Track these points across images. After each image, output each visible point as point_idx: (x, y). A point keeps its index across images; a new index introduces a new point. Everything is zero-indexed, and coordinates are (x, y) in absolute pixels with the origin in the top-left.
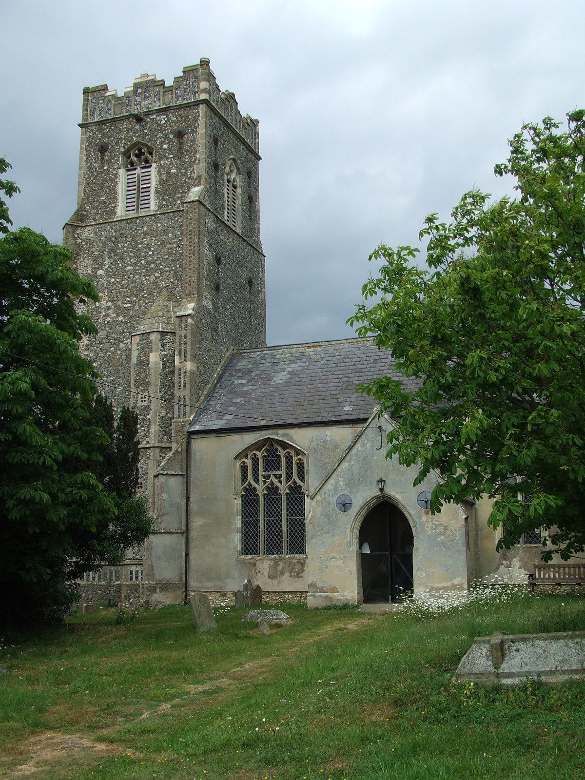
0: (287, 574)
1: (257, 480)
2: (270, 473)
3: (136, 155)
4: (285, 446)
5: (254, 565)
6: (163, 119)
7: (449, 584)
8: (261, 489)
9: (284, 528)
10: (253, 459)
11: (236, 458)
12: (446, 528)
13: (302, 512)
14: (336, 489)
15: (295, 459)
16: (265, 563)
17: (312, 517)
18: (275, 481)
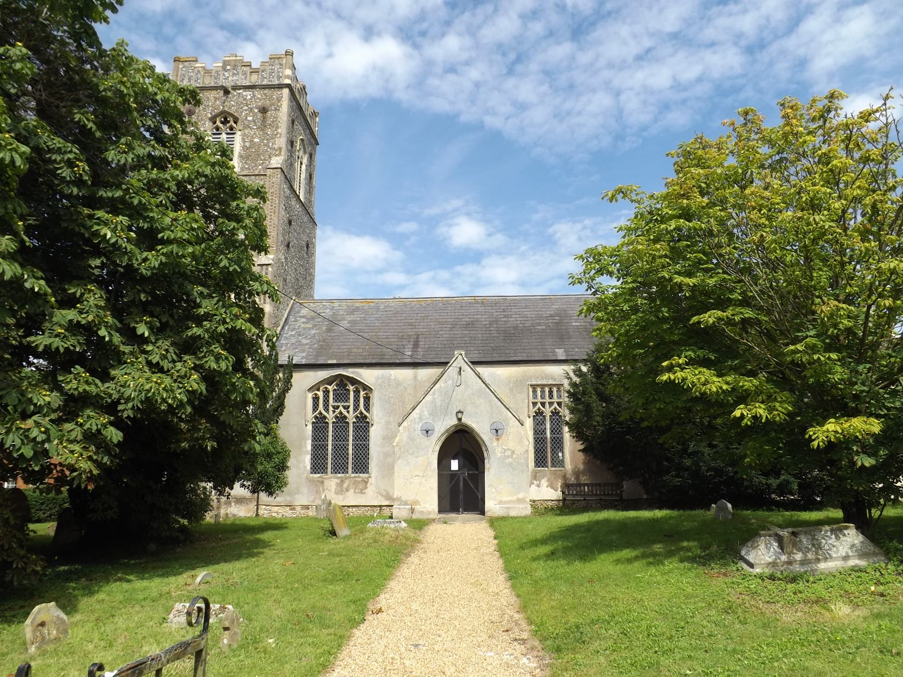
0: (352, 491)
2: (339, 404)
3: (222, 122)
4: (354, 381)
5: (322, 482)
6: (248, 94)
7: (515, 498)
8: (331, 417)
9: (350, 451)
10: (324, 392)
11: (309, 390)
12: (513, 452)
14: (420, 418)
15: (362, 393)
16: (331, 481)
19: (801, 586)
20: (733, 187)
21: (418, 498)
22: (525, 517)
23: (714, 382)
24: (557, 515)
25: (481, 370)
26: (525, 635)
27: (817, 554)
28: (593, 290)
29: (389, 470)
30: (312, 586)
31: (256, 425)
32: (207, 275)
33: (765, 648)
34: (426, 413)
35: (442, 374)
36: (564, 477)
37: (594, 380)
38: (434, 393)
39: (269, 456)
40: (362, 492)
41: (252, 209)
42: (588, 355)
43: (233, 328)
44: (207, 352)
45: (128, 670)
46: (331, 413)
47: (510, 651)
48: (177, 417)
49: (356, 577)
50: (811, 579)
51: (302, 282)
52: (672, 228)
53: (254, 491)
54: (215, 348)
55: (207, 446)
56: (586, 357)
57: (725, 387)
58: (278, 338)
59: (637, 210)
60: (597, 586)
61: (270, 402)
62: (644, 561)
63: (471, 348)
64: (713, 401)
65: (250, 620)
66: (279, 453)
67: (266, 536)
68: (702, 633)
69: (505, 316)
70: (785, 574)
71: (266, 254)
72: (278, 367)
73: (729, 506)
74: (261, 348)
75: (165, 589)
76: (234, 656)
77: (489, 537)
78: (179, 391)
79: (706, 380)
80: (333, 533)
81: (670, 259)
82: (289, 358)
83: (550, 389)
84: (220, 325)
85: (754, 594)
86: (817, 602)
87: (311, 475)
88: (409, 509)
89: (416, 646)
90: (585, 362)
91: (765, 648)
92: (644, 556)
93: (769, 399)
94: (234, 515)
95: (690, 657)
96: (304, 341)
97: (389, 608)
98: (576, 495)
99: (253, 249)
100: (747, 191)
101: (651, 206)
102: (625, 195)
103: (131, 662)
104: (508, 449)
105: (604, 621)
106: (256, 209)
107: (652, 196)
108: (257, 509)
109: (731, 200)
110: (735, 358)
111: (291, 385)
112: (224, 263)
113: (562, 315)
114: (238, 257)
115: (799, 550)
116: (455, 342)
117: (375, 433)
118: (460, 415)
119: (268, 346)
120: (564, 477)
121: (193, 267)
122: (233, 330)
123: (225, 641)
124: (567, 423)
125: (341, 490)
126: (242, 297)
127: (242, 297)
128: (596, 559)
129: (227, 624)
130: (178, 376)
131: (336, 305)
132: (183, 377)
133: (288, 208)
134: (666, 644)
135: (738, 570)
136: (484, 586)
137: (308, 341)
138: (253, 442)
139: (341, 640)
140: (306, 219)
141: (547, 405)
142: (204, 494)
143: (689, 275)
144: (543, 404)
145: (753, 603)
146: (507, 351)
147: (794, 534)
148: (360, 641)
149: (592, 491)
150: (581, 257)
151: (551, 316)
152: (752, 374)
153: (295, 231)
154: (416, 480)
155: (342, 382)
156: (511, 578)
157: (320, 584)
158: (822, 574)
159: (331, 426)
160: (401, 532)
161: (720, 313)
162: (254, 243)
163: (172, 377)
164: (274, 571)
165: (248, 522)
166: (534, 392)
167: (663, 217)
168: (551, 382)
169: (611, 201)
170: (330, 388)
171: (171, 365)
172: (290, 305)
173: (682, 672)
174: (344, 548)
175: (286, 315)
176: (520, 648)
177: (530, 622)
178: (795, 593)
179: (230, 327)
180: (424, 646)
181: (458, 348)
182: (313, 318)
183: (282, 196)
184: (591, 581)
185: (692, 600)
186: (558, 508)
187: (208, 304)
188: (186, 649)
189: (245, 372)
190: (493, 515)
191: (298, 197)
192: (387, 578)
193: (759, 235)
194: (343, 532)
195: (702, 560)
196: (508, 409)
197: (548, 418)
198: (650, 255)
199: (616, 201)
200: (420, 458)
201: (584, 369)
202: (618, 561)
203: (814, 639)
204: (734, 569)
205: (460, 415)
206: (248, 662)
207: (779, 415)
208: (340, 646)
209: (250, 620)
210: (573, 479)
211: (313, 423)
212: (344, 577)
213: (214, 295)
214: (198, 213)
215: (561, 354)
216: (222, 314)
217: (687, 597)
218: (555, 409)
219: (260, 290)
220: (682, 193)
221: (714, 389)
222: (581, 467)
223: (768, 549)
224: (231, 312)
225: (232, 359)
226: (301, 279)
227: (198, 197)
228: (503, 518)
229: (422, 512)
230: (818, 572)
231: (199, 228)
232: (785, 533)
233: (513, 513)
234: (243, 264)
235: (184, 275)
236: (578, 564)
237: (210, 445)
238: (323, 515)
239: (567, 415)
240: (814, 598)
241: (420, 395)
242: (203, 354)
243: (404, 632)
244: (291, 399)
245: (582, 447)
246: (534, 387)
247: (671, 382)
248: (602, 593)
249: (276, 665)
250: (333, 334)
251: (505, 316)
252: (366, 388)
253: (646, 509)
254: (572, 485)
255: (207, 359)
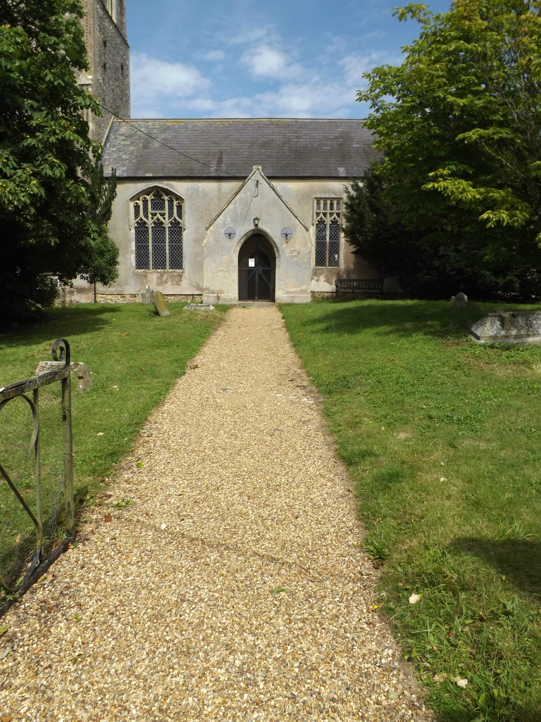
0: (170, 283)
1: (146, 216)
2: (156, 212)
4: (168, 192)
5: (146, 276)
7: (299, 289)
8: (150, 223)
9: (167, 251)
10: (143, 201)
11: (132, 199)
12: (299, 253)
13: (180, 241)
14: (224, 223)
15: (175, 203)
16: (153, 276)
17: (207, 242)
18: (161, 218)
19: (513, 353)
20: (510, 12)
21: (222, 288)
22: (306, 304)
23: (470, 191)
24: (332, 302)
25: (276, 184)
26: (305, 383)
27: (528, 330)
28: (377, 107)
29: (199, 267)
30: (143, 350)
31: (89, 224)
32: (35, 90)
33: (482, 392)
34: (228, 219)
35: (242, 187)
36: (338, 274)
37: (368, 194)
38: (235, 203)
39: (102, 253)
40: (178, 284)
41: (70, 24)
42: (365, 172)
43: (63, 138)
44: (42, 160)
45: (13, 388)
46: (150, 219)
47: (294, 393)
48: (23, 218)
49: (177, 344)
50: (521, 349)
51: (119, 102)
52: (452, 49)
53: (92, 281)
54: (49, 157)
55: (51, 242)
56: (362, 175)
57: (478, 196)
58: (102, 149)
59: (423, 30)
60: (360, 350)
61: (99, 209)
62: (397, 334)
63: (267, 165)
64: (466, 209)
65: (98, 373)
66: (110, 251)
67: (105, 316)
68: (437, 382)
69: (297, 137)
70: (502, 344)
71: (86, 71)
72: (104, 180)
73: (466, 297)
74: (88, 158)
75: (30, 354)
76: (88, 397)
77: (278, 318)
78: (23, 194)
79: (464, 189)
80: (157, 313)
81: (447, 80)
82: (113, 170)
83: (332, 202)
84: (51, 136)
85: (477, 358)
86: (523, 363)
87: (137, 270)
88: (215, 297)
89: (224, 390)
90: (362, 179)
91: (482, 392)
92: (397, 331)
93: (512, 208)
94: (77, 302)
95: (426, 397)
96: (125, 157)
97: (202, 365)
98: (347, 288)
99: (74, 65)
100: (523, 17)
101: (435, 27)
102: (414, 14)
103: (16, 382)
104: (295, 251)
105: (364, 374)
106: (74, 24)
107: (438, 17)
108: (95, 297)
109: (507, 26)
110: (489, 174)
111: (116, 194)
112: (49, 77)
113: (345, 138)
114: (61, 72)
115: (516, 327)
116: (253, 159)
117: (187, 236)
118: (256, 222)
119: (94, 156)
120: (338, 274)
121: (21, 81)
122: (63, 141)
123: (81, 386)
124: (343, 230)
125: (161, 282)
126: (68, 111)
127: (68, 111)
128: (360, 332)
129: (81, 374)
130: (20, 181)
131: (150, 124)
132: (25, 182)
133: (102, 30)
134: (409, 389)
135: (467, 341)
136: (274, 351)
137: (127, 157)
138: (88, 238)
139: (168, 387)
140: (119, 40)
141: (328, 215)
142: (51, 283)
143: (461, 96)
144: (325, 214)
145: (476, 363)
146: (297, 168)
147: (514, 316)
148: (182, 386)
149: (359, 285)
150: (368, 76)
151: (336, 138)
152: (500, 187)
153: (110, 52)
154: (221, 274)
155: (158, 192)
156: (295, 346)
157: (149, 349)
158: (529, 345)
159: (150, 230)
160: (210, 313)
161: (482, 131)
162: (75, 59)
163: (15, 183)
164: (112, 340)
165: (88, 307)
166: (318, 203)
167: (445, 38)
168: (332, 196)
169: (400, 19)
170: (148, 198)
171: (13, 171)
172: (110, 124)
173: (420, 406)
174: (166, 325)
175: (107, 133)
176: (301, 392)
177: (309, 374)
178: (508, 357)
179: (60, 138)
180: (230, 390)
181: (255, 164)
182: (131, 136)
183: (96, 16)
184: (356, 347)
185: (432, 361)
186: (332, 297)
187: (39, 116)
188: (54, 376)
189: (76, 179)
190: (282, 302)
191: (111, 18)
192: (201, 345)
193: (527, 58)
194: (165, 313)
195: (441, 334)
196: (296, 217)
197: (328, 226)
198: (430, 74)
199: (405, 20)
200: (224, 257)
201: (361, 185)
202: (378, 334)
203: (518, 387)
204: (465, 340)
205: (256, 222)
206: (99, 400)
207: (518, 220)
208: (167, 390)
209: (98, 373)
210: (345, 276)
211: (136, 227)
212: (168, 344)
213: (43, 108)
214: (20, 29)
215: (342, 171)
216: (51, 126)
217: (428, 358)
218: (335, 218)
219: (83, 104)
220: (465, 15)
221: (470, 197)
222: (352, 267)
223: (492, 326)
224: (59, 124)
225: (64, 167)
226: (118, 100)
227: (18, 12)
228: (289, 305)
229: (226, 299)
230: (527, 344)
231: (23, 42)
232: (507, 315)
233: (297, 301)
234: (66, 78)
235: (13, 89)
236: (346, 336)
237: (53, 242)
238: (148, 301)
239: (343, 223)
240: (521, 360)
241: (223, 204)
242: (39, 162)
243: (215, 381)
244: (117, 206)
245: (354, 250)
246: (318, 200)
247: (434, 191)
248: (364, 355)
249: (120, 402)
250: (149, 151)
251: (297, 137)
252: (178, 198)
253: (400, 299)
254: (344, 280)
255: (43, 167)
